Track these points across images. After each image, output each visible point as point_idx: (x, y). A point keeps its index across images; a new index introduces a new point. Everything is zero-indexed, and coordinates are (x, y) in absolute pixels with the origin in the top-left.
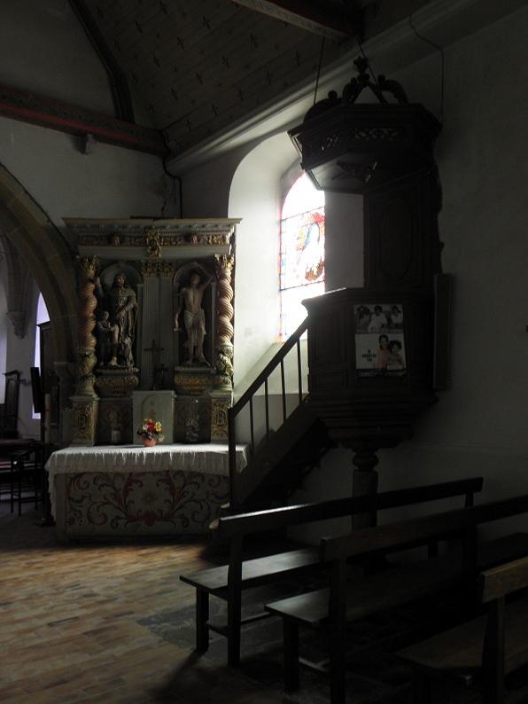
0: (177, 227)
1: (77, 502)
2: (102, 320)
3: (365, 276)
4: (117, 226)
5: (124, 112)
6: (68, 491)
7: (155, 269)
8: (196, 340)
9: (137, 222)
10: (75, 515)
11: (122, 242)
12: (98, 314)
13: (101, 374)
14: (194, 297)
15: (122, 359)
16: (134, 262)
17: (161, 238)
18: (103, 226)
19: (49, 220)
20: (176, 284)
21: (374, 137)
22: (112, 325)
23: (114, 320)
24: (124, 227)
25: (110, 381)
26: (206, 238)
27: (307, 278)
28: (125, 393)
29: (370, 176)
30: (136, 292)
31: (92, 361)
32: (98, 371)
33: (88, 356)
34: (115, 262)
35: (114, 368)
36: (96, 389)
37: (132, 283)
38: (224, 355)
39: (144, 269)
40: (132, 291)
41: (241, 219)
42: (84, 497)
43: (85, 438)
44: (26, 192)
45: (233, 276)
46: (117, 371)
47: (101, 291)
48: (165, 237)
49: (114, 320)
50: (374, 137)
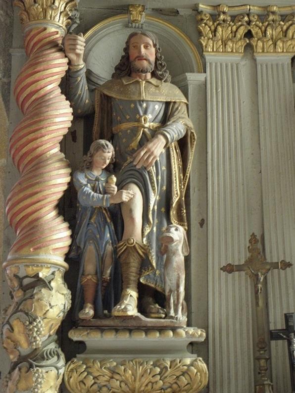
2: (90, 166)
7: (242, 31)
12: (78, 146)
13: (81, 347)
22: (121, 186)
23: (125, 169)
25: (113, 372)
31: (56, 301)
32: (75, 336)
33: (41, 283)
35: (128, 326)
39: (206, 30)
40: (178, 91)
46: (140, 339)
49: (125, 169)
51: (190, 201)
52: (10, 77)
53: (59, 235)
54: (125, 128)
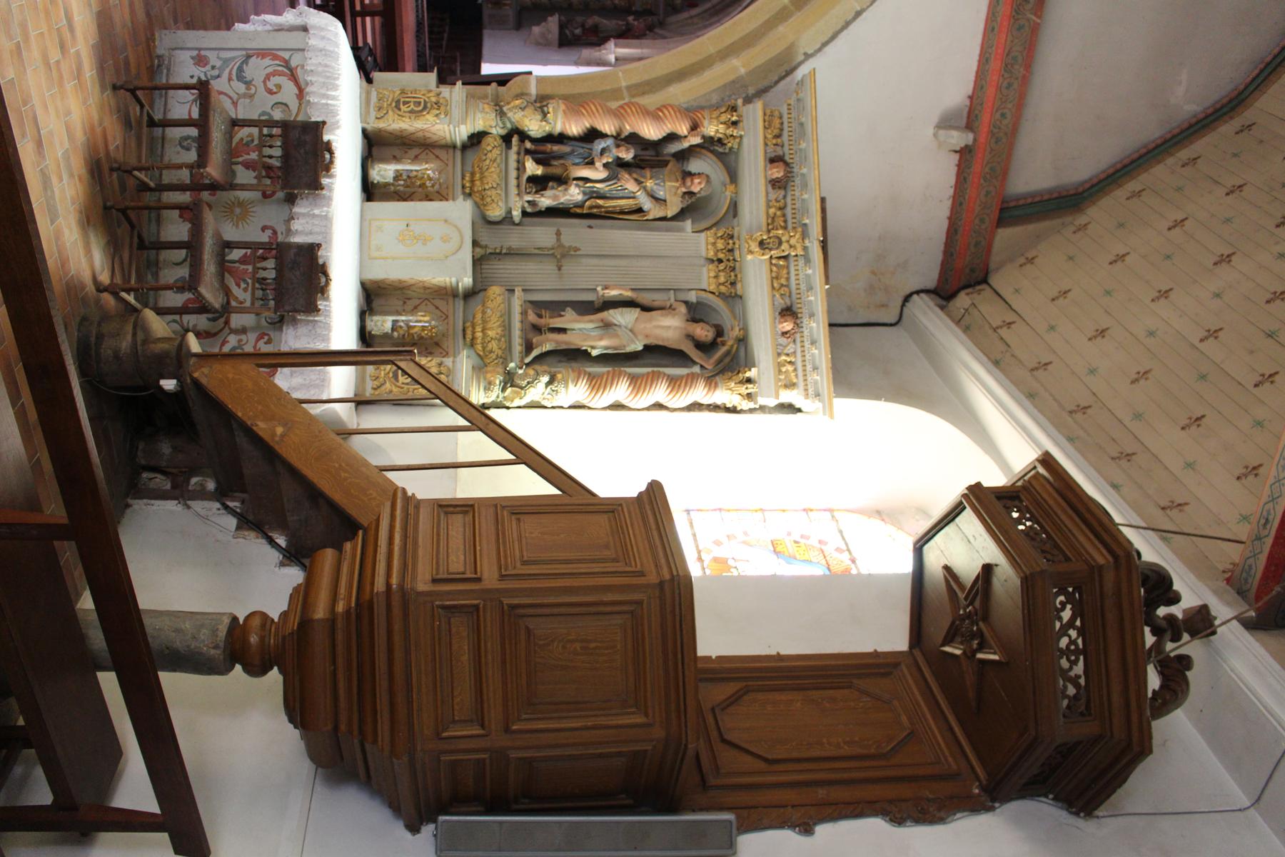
0: (810, 288)
1: (240, 70)
3: (720, 659)
4: (804, 171)
5: (1014, 212)
6: (263, 53)
7: (721, 256)
8: (583, 332)
9: (815, 207)
10: (213, 67)
11: (775, 183)
12: (633, 139)
14: (669, 328)
15: (539, 183)
16: (735, 215)
17: (785, 258)
18: (803, 145)
19: (808, 56)
20: (692, 297)
21: (1064, 642)
22: (605, 165)
24: (805, 186)
26: (790, 349)
27: (716, 560)
28: (470, 195)
29: (958, 652)
30: (674, 218)
34: (733, 176)
35: (521, 168)
36: (477, 139)
37: (693, 208)
38: (548, 384)
41: (832, 416)
42: (248, 84)
43: (380, 109)
44: (858, 14)
45: (715, 408)
46: (513, 174)
47: (674, 148)
48: (788, 267)
50: (1064, 642)
51: (781, 577)
52: (1238, 593)
53: (575, 129)
54: (628, 150)
